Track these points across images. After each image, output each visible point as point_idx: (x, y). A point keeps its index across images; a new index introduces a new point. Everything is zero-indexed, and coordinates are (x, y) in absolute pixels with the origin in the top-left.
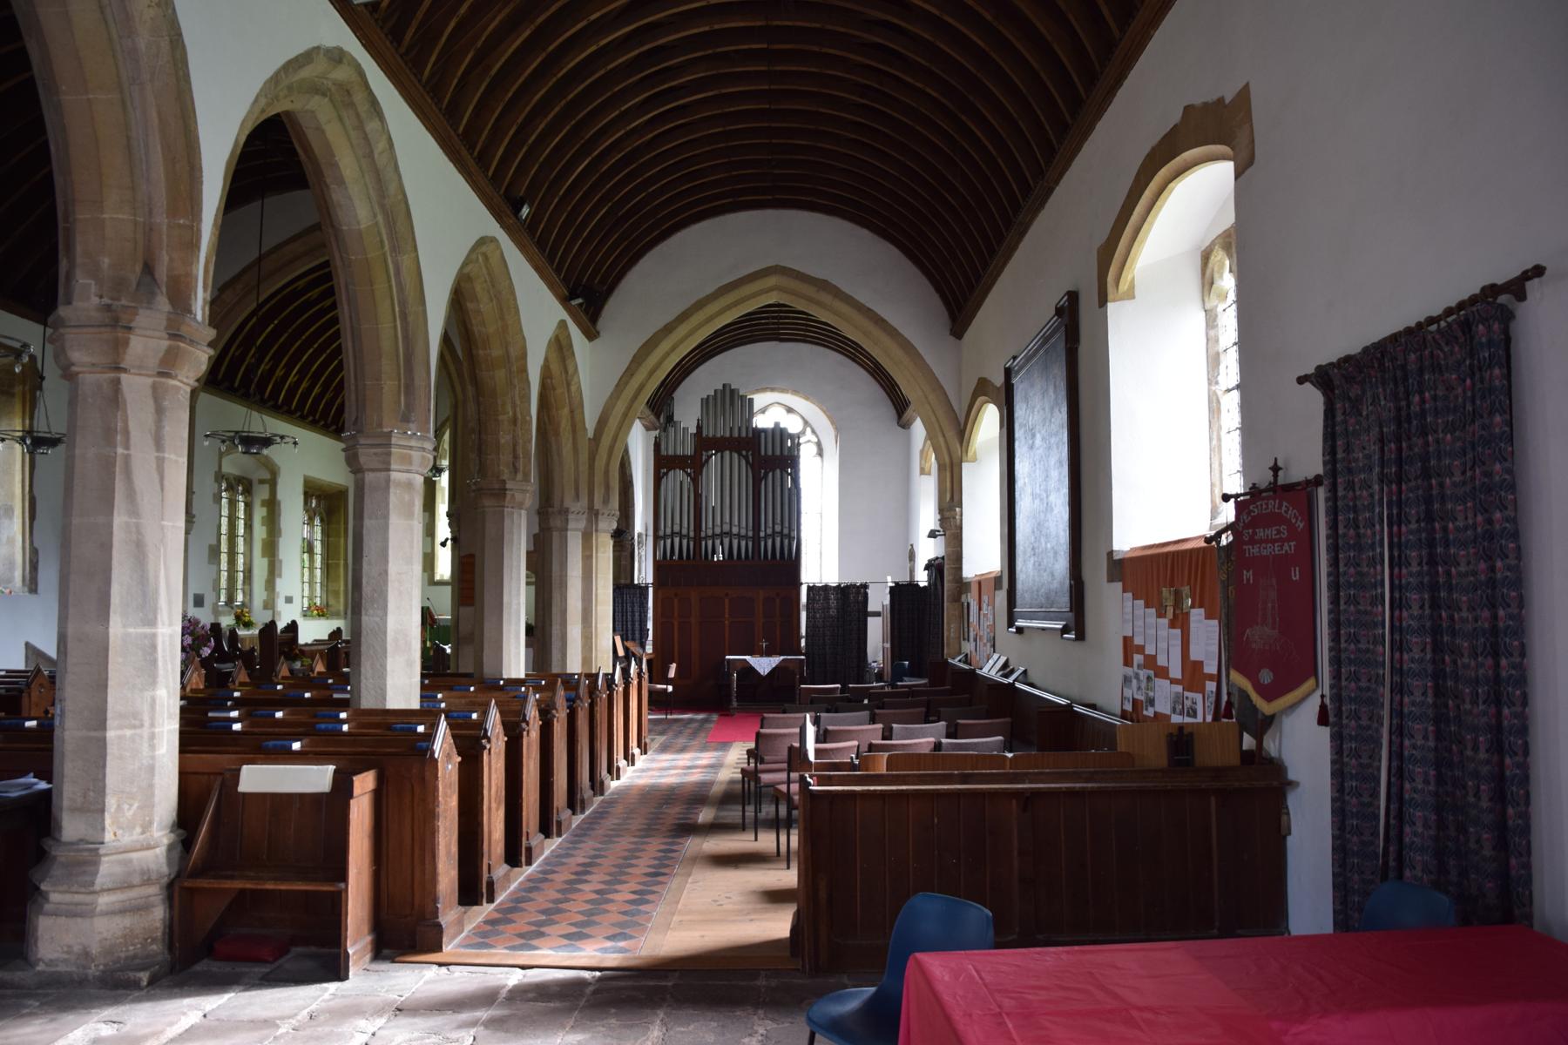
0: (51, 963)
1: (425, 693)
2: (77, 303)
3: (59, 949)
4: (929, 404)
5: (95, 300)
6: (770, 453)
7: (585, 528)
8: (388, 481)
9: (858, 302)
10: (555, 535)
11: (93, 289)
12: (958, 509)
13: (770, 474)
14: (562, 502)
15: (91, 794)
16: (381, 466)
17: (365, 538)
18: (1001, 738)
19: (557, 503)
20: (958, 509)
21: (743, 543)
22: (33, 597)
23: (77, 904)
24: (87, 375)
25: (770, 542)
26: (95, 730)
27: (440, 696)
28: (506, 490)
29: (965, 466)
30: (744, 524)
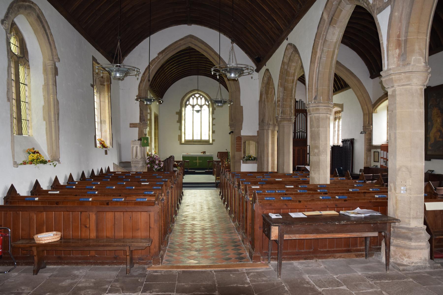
0: (416, 263)
1: (332, 178)
3: (418, 259)
4: (363, 96)
6: (303, 109)
9: (346, 67)
10: (265, 131)
12: (371, 126)
13: (299, 115)
17: (321, 134)
20: (371, 126)
23: (420, 246)
25: (299, 134)
26: (419, 194)
29: (374, 115)
30: (303, 129)
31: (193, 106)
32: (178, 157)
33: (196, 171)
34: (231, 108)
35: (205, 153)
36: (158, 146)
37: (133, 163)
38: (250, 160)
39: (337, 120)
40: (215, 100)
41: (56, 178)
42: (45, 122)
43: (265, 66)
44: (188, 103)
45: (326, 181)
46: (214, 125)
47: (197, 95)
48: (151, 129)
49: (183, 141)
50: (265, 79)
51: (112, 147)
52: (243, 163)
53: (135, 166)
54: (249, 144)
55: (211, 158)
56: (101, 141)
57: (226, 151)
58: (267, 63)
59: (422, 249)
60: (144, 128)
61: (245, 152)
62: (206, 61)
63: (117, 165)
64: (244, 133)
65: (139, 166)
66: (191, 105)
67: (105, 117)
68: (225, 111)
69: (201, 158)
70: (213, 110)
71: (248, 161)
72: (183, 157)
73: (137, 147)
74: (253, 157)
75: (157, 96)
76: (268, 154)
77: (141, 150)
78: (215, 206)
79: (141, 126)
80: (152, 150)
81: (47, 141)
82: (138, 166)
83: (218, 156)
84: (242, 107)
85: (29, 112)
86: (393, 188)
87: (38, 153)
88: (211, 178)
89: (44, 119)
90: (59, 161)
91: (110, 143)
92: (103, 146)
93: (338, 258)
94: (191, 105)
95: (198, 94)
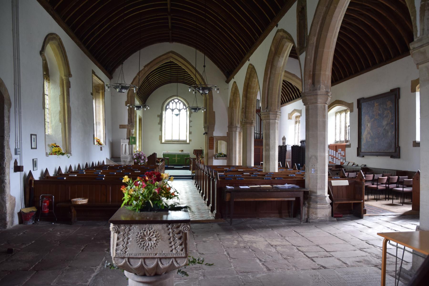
0: (320, 218)
2: (321, 90)
5: (325, 90)
8: (275, 122)
10: (234, 132)
11: (324, 87)
14: (236, 125)
15: (323, 186)
16: (274, 119)
18: (407, 176)
19: (234, 125)
21: (257, 135)
23: (323, 207)
24: (319, 104)
27: (85, 173)
30: (257, 130)
31: (173, 110)
32: (160, 155)
33: (175, 167)
34: (205, 113)
35: (183, 151)
36: (143, 145)
37: (123, 158)
38: (221, 157)
39: (298, 124)
41: (60, 169)
42: (61, 124)
43: (233, 79)
44: (168, 107)
45: (275, 170)
46: (191, 127)
47: (176, 101)
48: (136, 130)
49: (163, 141)
50: (234, 89)
51: (106, 144)
52: (215, 159)
53: (124, 161)
54: (221, 144)
55: (188, 155)
57: (201, 149)
58: (250, 58)
59: (324, 209)
60: (132, 129)
61: (217, 151)
62: (184, 71)
63: (109, 159)
64: (216, 134)
65: (128, 161)
66: (171, 109)
67: (100, 119)
68: (201, 115)
69: (179, 155)
70: (190, 113)
71: (219, 158)
72: (163, 155)
73: (126, 145)
75: (141, 101)
78: (191, 191)
79: (130, 127)
80: (137, 148)
81: (62, 138)
82: (127, 161)
83: (194, 153)
84: (214, 112)
85: (49, 116)
86: (307, 170)
87: (59, 147)
88: (189, 173)
89: (61, 122)
90: (71, 154)
92: (100, 144)
93: (273, 217)
94: (171, 109)
95: (177, 99)
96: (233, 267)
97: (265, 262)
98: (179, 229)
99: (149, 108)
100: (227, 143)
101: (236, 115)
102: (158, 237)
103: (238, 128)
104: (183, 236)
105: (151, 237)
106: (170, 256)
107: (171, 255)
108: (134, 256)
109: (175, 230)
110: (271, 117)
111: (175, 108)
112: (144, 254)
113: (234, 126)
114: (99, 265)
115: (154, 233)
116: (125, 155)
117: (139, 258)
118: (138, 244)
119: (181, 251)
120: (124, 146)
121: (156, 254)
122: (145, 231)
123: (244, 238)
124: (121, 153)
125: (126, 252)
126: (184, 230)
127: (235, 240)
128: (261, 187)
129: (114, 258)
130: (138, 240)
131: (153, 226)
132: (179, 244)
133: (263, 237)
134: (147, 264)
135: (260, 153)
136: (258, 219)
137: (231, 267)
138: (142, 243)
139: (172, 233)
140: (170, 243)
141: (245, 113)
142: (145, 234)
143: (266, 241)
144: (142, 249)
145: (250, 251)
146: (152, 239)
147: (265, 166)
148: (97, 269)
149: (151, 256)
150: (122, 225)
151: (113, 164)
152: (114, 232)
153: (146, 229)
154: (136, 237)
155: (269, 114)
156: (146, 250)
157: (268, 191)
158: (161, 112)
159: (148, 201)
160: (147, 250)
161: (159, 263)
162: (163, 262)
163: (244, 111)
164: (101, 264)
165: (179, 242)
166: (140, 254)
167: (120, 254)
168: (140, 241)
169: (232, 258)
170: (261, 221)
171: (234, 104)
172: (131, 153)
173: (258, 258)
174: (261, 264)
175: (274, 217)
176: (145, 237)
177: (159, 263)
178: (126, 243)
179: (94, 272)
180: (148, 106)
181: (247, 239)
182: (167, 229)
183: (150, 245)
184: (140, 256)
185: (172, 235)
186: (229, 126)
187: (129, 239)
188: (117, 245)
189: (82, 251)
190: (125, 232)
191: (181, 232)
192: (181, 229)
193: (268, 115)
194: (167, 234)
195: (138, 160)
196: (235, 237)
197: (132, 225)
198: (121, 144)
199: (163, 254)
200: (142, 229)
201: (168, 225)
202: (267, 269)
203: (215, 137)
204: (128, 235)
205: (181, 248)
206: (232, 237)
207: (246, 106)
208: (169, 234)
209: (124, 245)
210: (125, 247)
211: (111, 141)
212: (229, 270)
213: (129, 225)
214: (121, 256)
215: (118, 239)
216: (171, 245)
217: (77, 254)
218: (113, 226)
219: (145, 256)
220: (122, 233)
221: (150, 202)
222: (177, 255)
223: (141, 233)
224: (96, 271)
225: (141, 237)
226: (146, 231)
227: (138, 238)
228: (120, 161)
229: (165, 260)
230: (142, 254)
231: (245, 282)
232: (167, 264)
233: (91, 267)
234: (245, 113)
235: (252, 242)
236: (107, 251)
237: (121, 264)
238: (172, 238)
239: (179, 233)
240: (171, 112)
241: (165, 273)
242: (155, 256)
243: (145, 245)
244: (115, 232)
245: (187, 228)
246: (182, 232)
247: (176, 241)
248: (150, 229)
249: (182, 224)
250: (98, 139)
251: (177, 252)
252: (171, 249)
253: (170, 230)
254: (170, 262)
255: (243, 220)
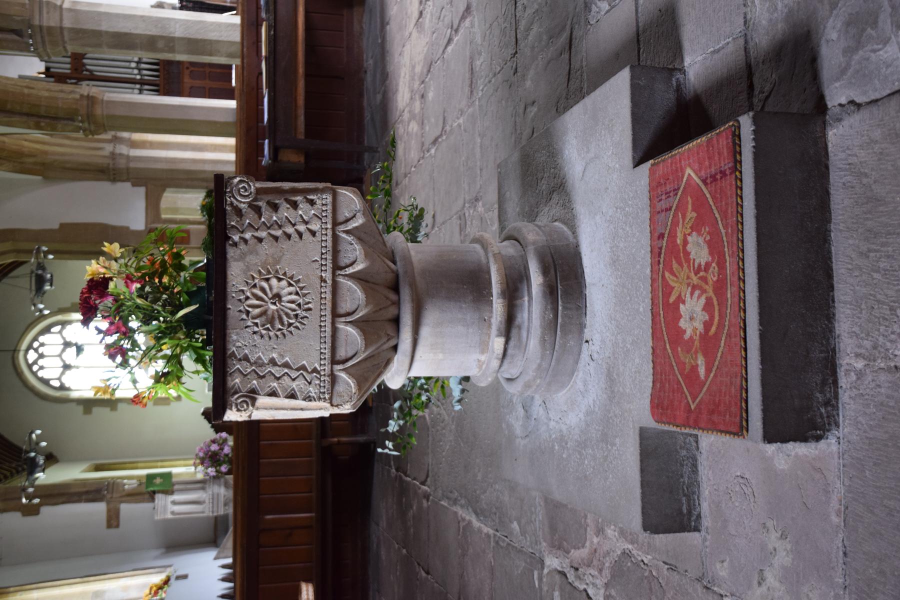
7: (127, 146)
8: (70, 10)
10: (132, 165)
13: (88, 67)
17: (116, 30)
19: (106, 161)
22: (189, 577)
25: (145, 72)
28: (88, 95)
31: (67, 367)
34: (60, 254)
36: (177, 455)
37: (215, 509)
40: (34, 293)
44: (56, 384)
45: (235, 25)
51: (170, 566)
54: (176, 210)
56: (150, 594)
66: (63, 373)
73: (174, 503)
74: (204, 200)
76: (194, 161)
77: (181, 491)
82: (224, 496)
84: (62, 225)
91: (161, 572)
92: (167, 582)
93: (362, 28)
95: (27, 351)
96: (461, 121)
97: (452, 28)
98: (244, 211)
99: (39, 432)
100: (170, 186)
101: (72, 155)
102: (269, 273)
103: (118, 151)
104: (269, 197)
105: (270, 295)
106: (329, 238)
107: (326, 234)
108: (328, 345)
109: (248, 221)
110: (52, 24)
111: (58, 358)
112: (321, 316)
113: (111, 162)
114: (456, 513)
115: (255, 286)
116: (207, 501)
117: (335, 330)
118: (291, 332)
119: (316, 207)
120: (177, 508)
121: (323, 280)
122: (248, 313)
123: (405, 104)
124: (201, 515)
125: (315, 370)
126: (247, 194)
127: (408, 128)
128: (266, 57)
129: (332, 405)
130: (278, 333)
131: (234, 289)
132: (291, 210)
133: (404, 46)
134: (354, 307)
135: (204, 88)
136: (366, 72)
137: (459, 126)
138: (286, 323)
139: (257, 230)
140: (289, 237)
141: (56, 118)
142: (257, 311)
143: (410, 34)
144: (305, 321)
145: (430, 79)
146: (275, 291)
147: (221, 56)
148: (464, 515)
149: (329, 296)
150: (230, 383)
151: (228, 542)
152: (251, 408)
153: (242, 308)
154: (267, 339)
155: (41, 27)
156: (310, 309)
157: (274, 31)
158: (74, 404)
159: (178, 321)
160: (310, 305)
161: (350, 270)
162: (348, 262)
163: (48, 121)
164: (454, 509)
165: (285, 211)
166: (321, 326)
167: (320, 386)
168: (280, 327)
169: (443, 129)
170: (371, 62)
171: (31, 160)
172: (202, 484)
173: (444, 52)
174: (457, 38)
175: (360, 22)
176: (270, 313)
177: (350, 270)
178: (286, 370)
179: (470, 523)
180: (32, 432)
181: (405, 94)
182: (242, 246)
183: (294, 297)
184: (328, 329)
185: (262, 231)
186: (112, 178)
187: (273, 362)
188: (292, 396)
189: (428, 573)
190: (253, 373)
191: (255, 203)
192: (244, 203)
193: (45, 31)
194: (260, 245)
195: (224, 462)
196: (403, 130)
197: (229, 352)
198: (170, 516)
199: (322, 259)
200: (242, 322)
201: (231, 242)
202: (466, 18)
203: (149, 226)
204: (262, 365)
205: (303, 206)
206: (401, 140)
207: (28, 115)
208: (260, 240)
209: (294, 374)
210: (298, 374)
211: (163, 550)
212: (465, 131)
213: (229, 361)
214: (327, 385)
215: (273, 394)
216: (295, 236)
217: (436, 585)
218: (231, 409)
219: (328, 313)
220: (255, 382)
221: (181, 313)
222: (326, 216)
223: (256, 324)
224: (467, 518)
225: (269, 326)
226: (250, 309)
227: (271, 334)
228: (226, 517)
229: (342, 255)
230: (321, 321)
231: (491, 76)
232: (355, 250)
233: (459, 535)
234: (56, 118)
235: (412, 79)
236: (428, 500)
237: (352, 384)
238: (273, 232)
239: (258, 211)
240: (73, 370)
241: (394, 263)
242: (328, 282)
243: (292, 313)
244: (253, 405)
245: (241, 186)
246: (255, 200)
247: (284, 219)
248: (242, 297)
249: (228, 199)
250: (148, 591)
251: (316, 218)
252: (307, 236)
253: (248, 235)
254: (350, 238)
255: (367, 116)
